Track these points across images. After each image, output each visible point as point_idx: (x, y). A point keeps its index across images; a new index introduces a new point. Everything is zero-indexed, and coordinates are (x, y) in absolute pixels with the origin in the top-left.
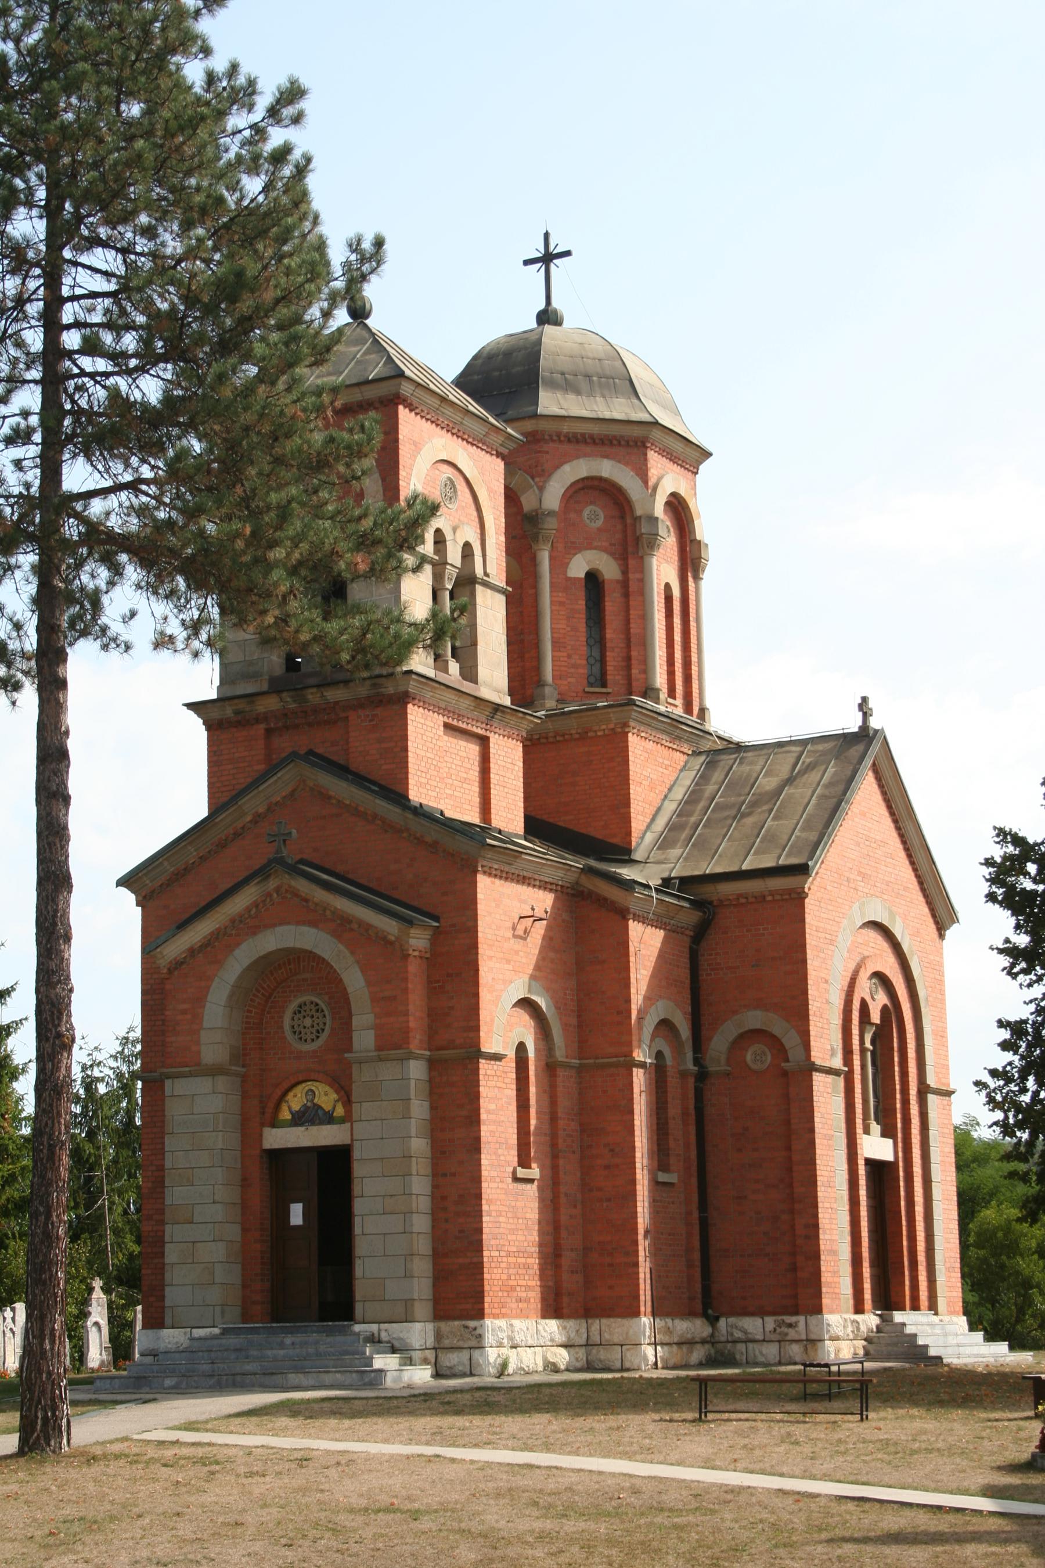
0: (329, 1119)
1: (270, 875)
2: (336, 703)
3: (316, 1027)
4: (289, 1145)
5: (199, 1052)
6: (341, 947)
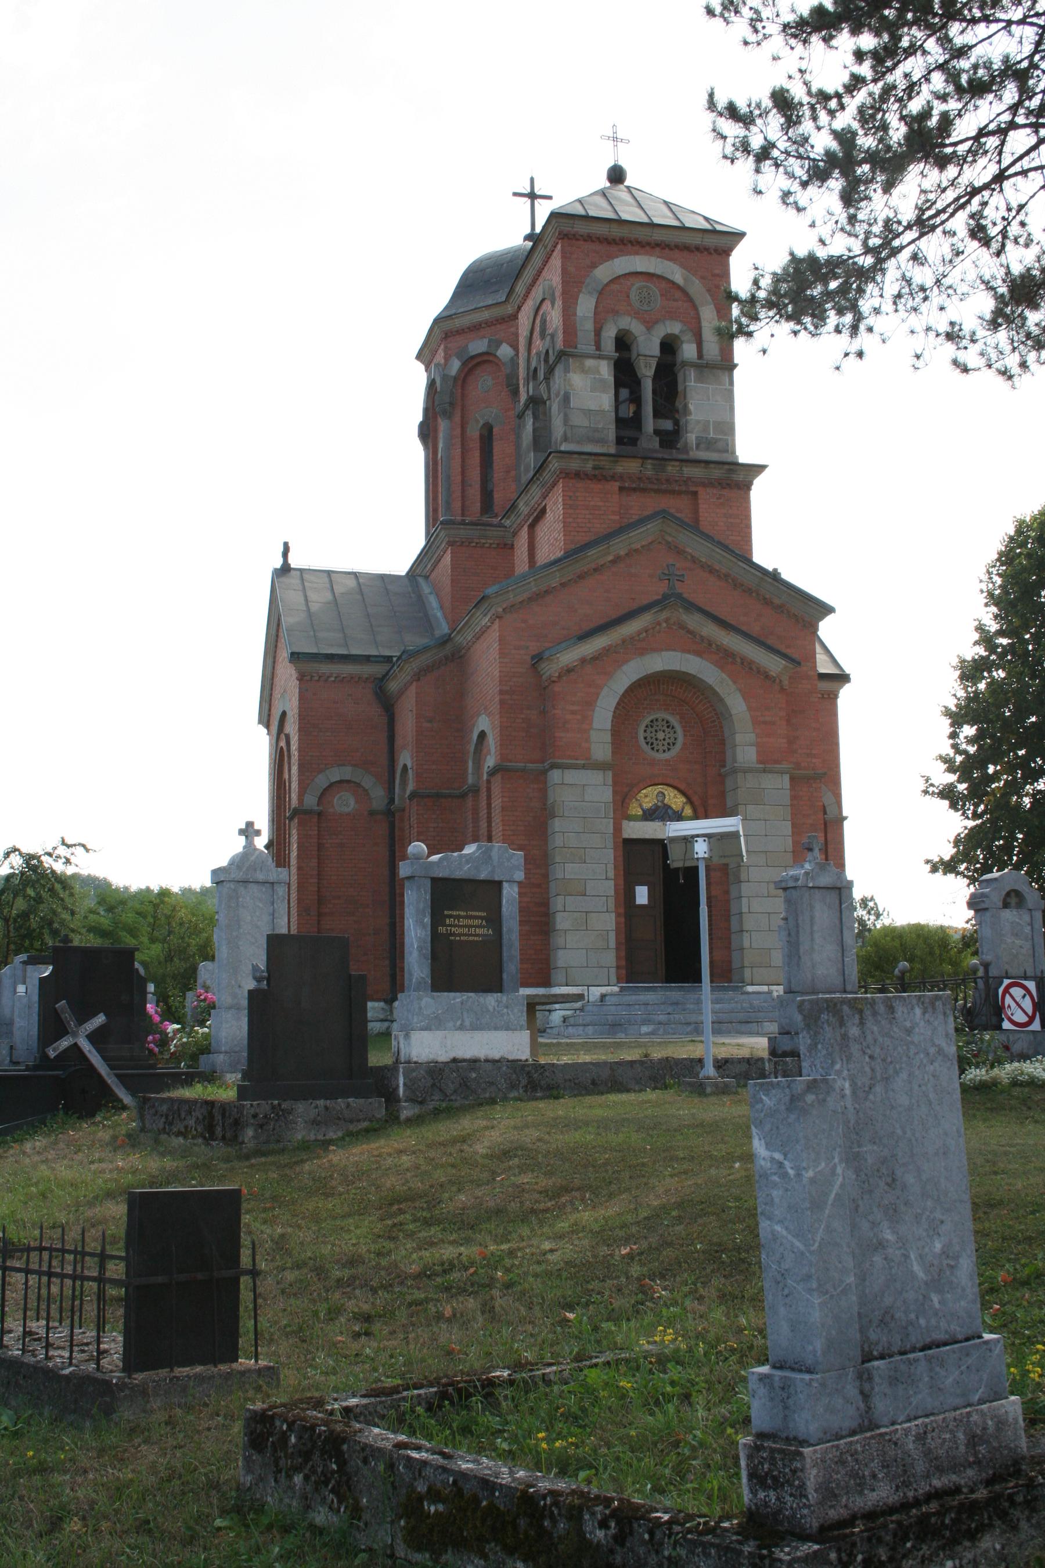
0: (679, 817)
2: (689, 478)
3: (668, 740)
4: (647, 837)
5: (589, 749)
6: (724, 676)
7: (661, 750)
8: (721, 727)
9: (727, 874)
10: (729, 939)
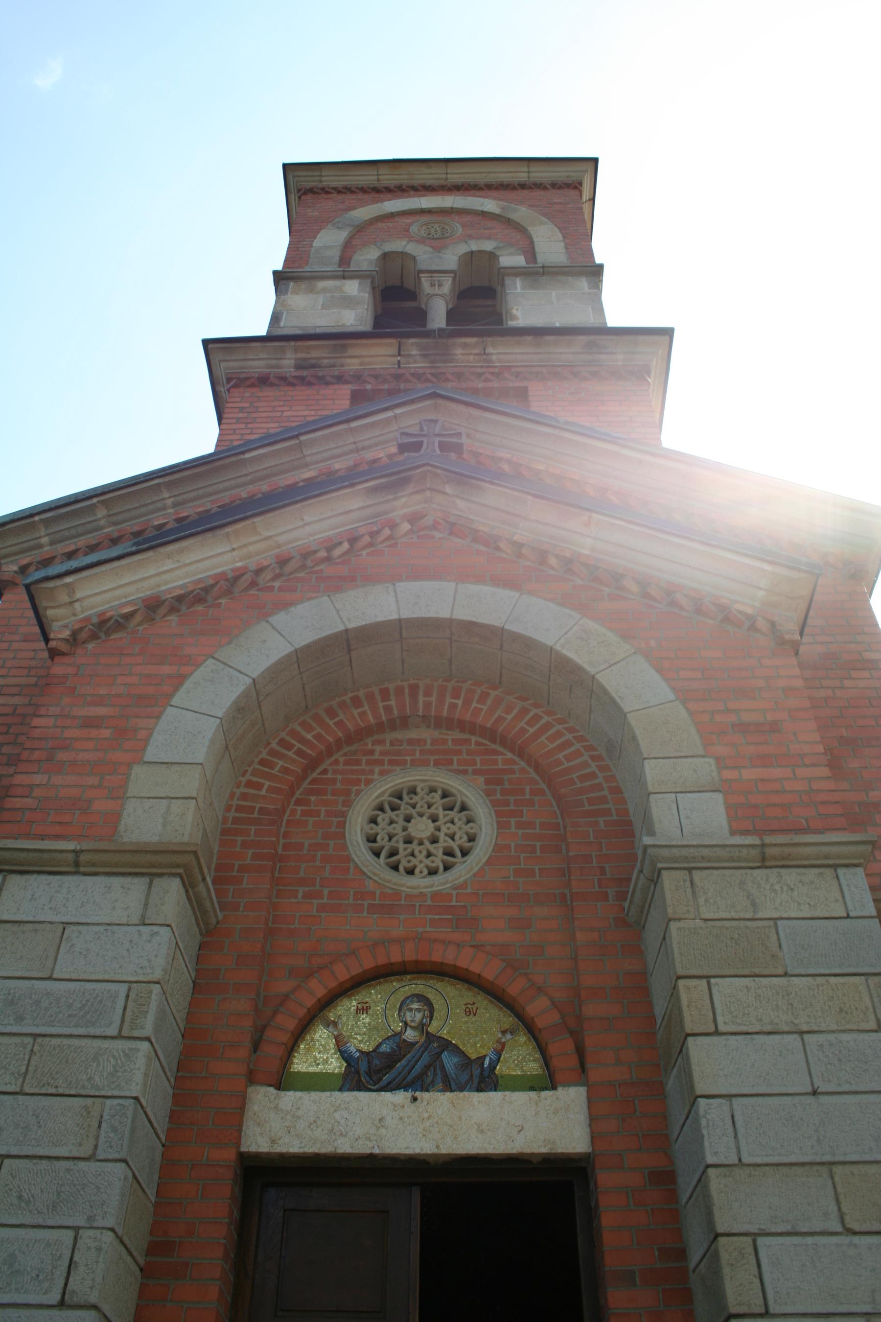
1: (406, 481)
3: (444, 842)
4: (344, 1146)
8: (617, 790)
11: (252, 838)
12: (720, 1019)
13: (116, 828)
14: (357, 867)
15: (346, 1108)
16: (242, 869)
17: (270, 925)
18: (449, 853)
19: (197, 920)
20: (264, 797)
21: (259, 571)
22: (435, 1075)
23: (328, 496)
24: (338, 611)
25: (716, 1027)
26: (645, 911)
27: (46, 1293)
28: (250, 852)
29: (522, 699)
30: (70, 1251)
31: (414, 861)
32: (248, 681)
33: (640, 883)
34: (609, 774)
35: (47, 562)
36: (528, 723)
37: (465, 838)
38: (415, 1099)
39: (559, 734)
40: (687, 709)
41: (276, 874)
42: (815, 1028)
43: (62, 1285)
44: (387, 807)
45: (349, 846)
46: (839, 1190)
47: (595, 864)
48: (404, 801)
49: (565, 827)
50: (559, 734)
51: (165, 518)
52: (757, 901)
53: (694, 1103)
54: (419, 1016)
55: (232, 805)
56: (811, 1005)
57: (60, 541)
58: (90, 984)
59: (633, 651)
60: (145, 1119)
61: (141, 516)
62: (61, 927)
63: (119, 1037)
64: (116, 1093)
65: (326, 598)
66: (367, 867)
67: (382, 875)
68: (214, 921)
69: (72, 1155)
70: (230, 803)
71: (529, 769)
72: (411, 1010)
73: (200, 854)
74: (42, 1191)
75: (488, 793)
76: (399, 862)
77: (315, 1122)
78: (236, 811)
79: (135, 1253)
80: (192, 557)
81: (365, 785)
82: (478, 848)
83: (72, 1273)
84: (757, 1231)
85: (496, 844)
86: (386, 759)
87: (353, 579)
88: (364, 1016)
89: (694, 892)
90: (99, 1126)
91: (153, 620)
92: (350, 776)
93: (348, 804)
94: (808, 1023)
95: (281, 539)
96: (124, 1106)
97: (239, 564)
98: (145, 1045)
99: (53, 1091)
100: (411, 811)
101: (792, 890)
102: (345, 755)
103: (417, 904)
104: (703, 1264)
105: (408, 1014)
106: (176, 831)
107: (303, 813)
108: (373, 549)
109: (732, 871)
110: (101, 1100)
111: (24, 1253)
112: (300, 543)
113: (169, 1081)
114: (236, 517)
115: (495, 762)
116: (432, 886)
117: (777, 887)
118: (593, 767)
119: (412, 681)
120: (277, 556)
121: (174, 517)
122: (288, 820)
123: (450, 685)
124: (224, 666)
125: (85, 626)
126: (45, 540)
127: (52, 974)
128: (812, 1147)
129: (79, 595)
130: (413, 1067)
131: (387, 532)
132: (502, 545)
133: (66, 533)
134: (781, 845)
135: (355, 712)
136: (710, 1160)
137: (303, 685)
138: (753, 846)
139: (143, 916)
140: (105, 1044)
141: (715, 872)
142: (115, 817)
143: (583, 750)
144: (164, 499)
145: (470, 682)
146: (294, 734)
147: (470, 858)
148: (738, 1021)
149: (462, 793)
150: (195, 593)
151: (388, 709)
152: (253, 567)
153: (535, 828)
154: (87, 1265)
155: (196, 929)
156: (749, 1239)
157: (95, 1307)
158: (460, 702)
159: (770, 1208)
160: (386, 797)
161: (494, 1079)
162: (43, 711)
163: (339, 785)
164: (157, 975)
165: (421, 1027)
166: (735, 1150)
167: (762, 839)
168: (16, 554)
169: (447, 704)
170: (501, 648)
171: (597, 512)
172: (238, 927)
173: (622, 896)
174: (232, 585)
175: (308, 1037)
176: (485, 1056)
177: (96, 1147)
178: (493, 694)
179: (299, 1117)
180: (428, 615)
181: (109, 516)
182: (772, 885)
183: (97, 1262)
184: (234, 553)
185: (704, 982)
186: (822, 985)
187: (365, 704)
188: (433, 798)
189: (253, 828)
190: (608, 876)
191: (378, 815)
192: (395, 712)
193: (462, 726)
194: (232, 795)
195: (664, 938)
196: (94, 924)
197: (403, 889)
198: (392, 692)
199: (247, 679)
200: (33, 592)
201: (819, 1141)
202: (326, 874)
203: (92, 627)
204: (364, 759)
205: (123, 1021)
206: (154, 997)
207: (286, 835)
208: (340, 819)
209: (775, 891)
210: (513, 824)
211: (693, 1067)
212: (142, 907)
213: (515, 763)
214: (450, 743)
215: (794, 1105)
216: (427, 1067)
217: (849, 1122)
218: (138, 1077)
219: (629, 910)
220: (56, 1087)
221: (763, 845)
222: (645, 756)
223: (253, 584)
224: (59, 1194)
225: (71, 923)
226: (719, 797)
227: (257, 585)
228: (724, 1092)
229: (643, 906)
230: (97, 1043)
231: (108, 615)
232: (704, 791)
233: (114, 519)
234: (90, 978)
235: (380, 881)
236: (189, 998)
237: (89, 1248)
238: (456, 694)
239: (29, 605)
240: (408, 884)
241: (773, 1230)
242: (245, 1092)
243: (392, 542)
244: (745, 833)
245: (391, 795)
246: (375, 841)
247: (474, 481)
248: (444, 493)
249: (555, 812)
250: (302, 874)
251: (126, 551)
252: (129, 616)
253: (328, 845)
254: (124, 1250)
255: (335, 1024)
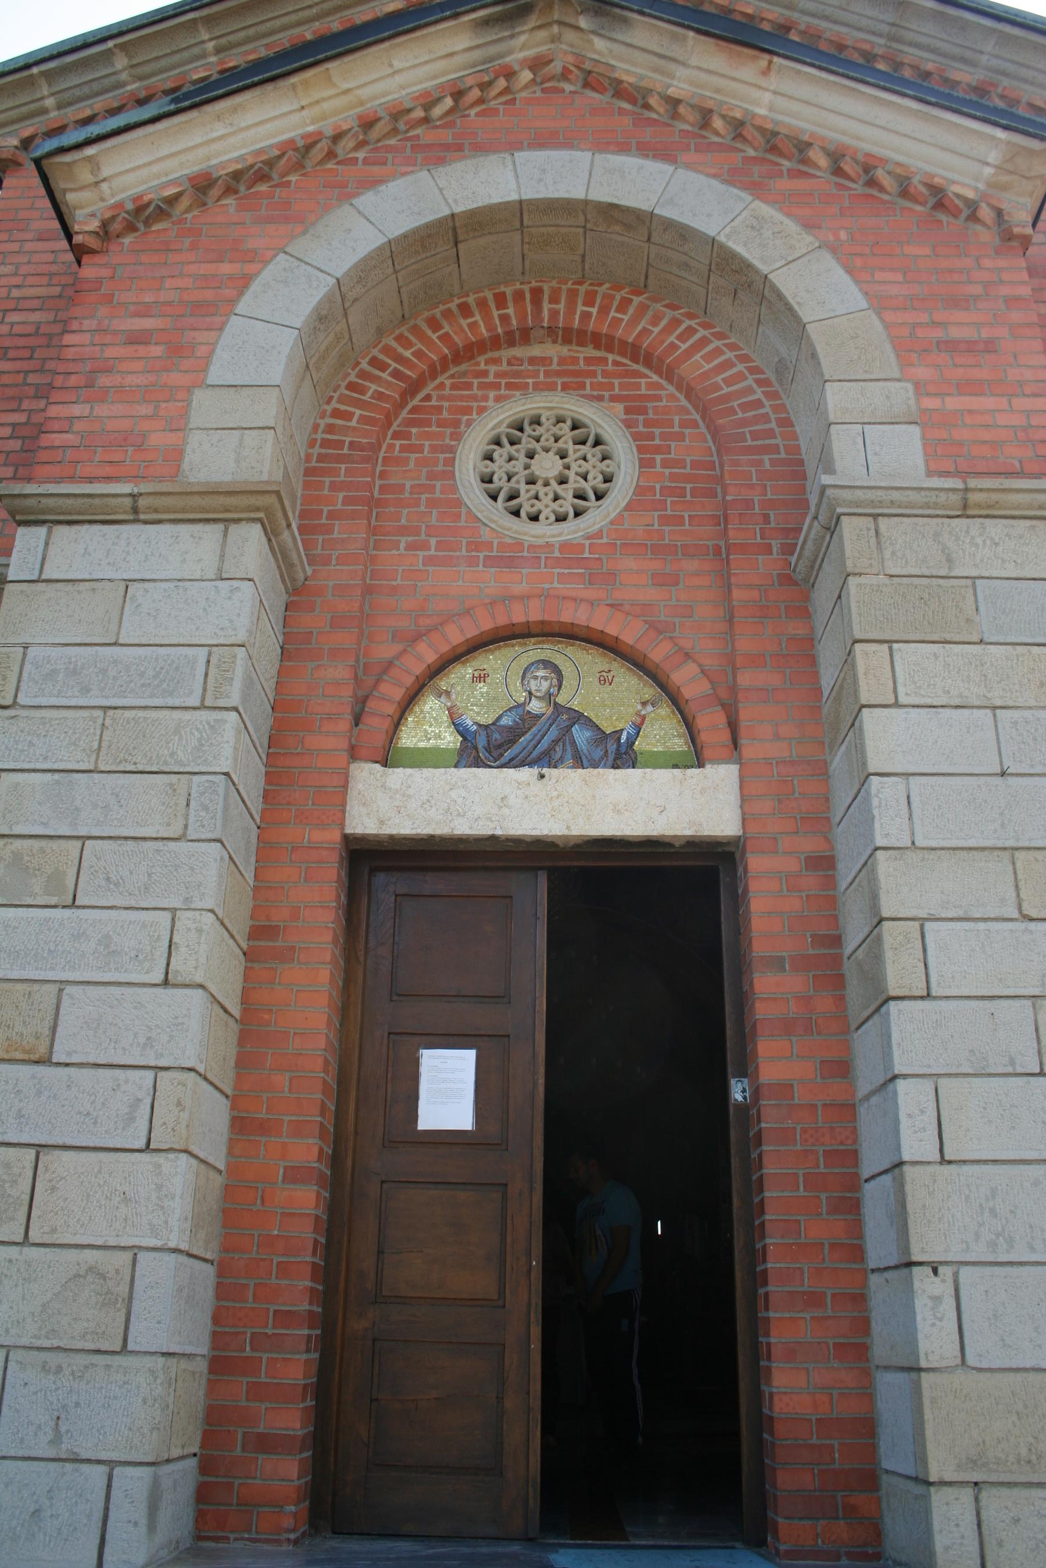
3: (575, 482)
7: (489, 467)
8: (786, 423)
9: (839, 981)
10: (860, 1299)
11: (342, 478)
12: (901, 690)
13: (179, 466)
14: (469, 512)
15: (463, 787)
16: (332, 516)
17: (368, 581)
18: (581, 496)
19: (282, 576)
20: (354, 429)
21: (336, 138)
22: (564, 750)
23: (425, 31)
24: (441, 190)
25: (896, 698)
26: (817, 566)
27: (147, 973)
28: (341, 495)
29: (672, 307)
30: (169, 933)
31: (539, 505)
32: (332, 281)
33: (813, 532)
34: (778, 402)
35: (59, 130)
36: (679, 338)
37: (600, 478)
38: (542, 776)
39: (718, 352)
40: (882, 320)
41: (373, 523)
42: (1011, 703)
43: (165, 965)
44: (505, 441)
45: (460, 487)
46: (1020, 876)
47: (757, 511)
48: (526, 433)
49: (722, 466)
50: (718, 352)
51: (205, 70)
52: (954, 555)
53: (865, 782)
54: (545, 685)
55: (315, 440)
56: (1008, 677)
57: (70, 104)
58: (163, 648)
59: (817, 244)
60: (238, 797)
61: (173, 67)
62: (123, 585)
63: (203, 707)
64: (203, 769)
65: (425, 173)
66: (481, 512)
67: (501, 522)
68: (301, 577)
69: (160, 835)
70: (314, 436)
71: (678, 395)
72: (536, 678)
73: (283, 494)
74: (131, 873)
75: (628, 424)
76: (520, 506)
77: (428, 801)
78: (322, 446)
79: (237, 937)
80: (249, 118)
81: (478, 414)
82: (616, 491)
83: (173, 954)
84: (925, 916)
85: (637, 486)
86: (503, 382)
87: (460, 148)
88: (482, 684)
89: (878, 543)
90: (188, 805)
91: (205, 204)
92: (459, 403)
93: (457, 437)
94: (1002, 697)
95: (365, 93)
96: (213, 782)
97: (311, 129)
98: (234, 715)
99: (132, 768)
100: (534, 445)
101: (997, 544)
102: (452, 376)
103: (543, 556)
104: (861, 949)
105: (533, 683)
106: (253, 468)
107: (404, 449)
108: (483, 107)
109: (926, 520)
110: (187, 776)
111: (119, 935)
112: (389, 98)
113: (260, 757)
114: (304, 62)
115: (638, 386)
116: (560, 535)
117: (979, 541)
118: (759, 394)
119: (534, 284)
120: (360, 117)
121: (219, 68)
122: (384, 458)
123: (582, 289)
124: (299, 263)
125: (118, 215)
126: (50, 102)
127: (118, 638)
128: (995, 831)
129: (106, 172)
130: (539, 742)
131: (502, 83)
132: (653, 101)
133: (77, 92)
134: (988, 490)
135: (464, 323)
136: (880, 842)
137: (399, 288)
138: (954, 490)
139: (220, 570)
140: (187, 715)
141: (905, 519)
142: (177, 454)
143: (746, 372)
144: (203, 42)
145: (607, 285)
146: (387, 350)
147: (605, 502)
148: (922, 692)
149: (596, 422)
150: (256, 167)
151: (505, 319)
152: (329, 132)
153: (685, 467)
154: (188, 946)
155: (281, 586)
156: (916, 924)
157: (201, 986)
158: (594, 311)
159: (942, 892)
160: (503, 429)
161: (633, 756)
162: (75, 325)
163: (445, 415)
164: (241, 637)
165: (549, 697)
166: (908, 832)
167: (965, 482)
168: (13, 122)
169: (578, 313)
170: (649, 240)
171: (778, 55)
172: (331, 583)
173: (789, 549)
174: (303, 157)
175: (417, 709)
176: (622, 730)
177: (186, 827)
178: (636, 300)
179: (409, 797)
180: (556, 195)
181: (132, 66)
182: (973, 538)
183: (199, 943)
184: (304, 113)
185: (885, 647)
186: (1023, 655)
187: (477, 313)
188: (561, 429)
189: (343, 466)
190: (773, 525)
191: (494, 450)
192: (514, 322)
193: (596, 340)
194: (316, 427)
195: (839, 597)
196: (161, 580)
197: (526, 538)
198: (509, 298)
199: (329, 278)
200: (46, 170)
201: (1003, 825)
202: (434, 522)
203: (126, 216)
204: (476, 381)
205: (205, 690)
206: (239, 662)
207: (383, 475)
208: (448, 455)
209: (977, 546)
210: (658, 462)
211: (867, 742)
212: (217, 558)
213: (662, 388)
214: (582, 362)
215: (979, 786)
216: (556, 742)
217: (1038, 805)
218: (228, 751)
219: (795, 566)
220: (135, 764)
221: (966, 490)
222: (827, 377)
223: (331, 155)
224: (149, 875)
225: (135, 581)
226: (915, 431)
227: (336, 156)
228: (900, 771)
229: (815, 560)
230: (177, 715)
231: (146, 199)
232: (897, 423)
233: (140, 70)
234: (163, 643)
235: (499, 530)
236: (277, 666)
237: (189, 929)
238: (589, 301)
239: (42, 191)
240: (531, 533)
241: (943, 915)
242: (347, 769)
243: (509, 97)
244: (945, 474)
245: (509, 426)
246: (490, 481)
247: (618, 11)
248: (578, 28)
249: (710, 448)
250: (403, 521)
251: (161, 111)
252: (172, 200)
253: (434, 486)
254: (226, 934)
255: (448, 693)
